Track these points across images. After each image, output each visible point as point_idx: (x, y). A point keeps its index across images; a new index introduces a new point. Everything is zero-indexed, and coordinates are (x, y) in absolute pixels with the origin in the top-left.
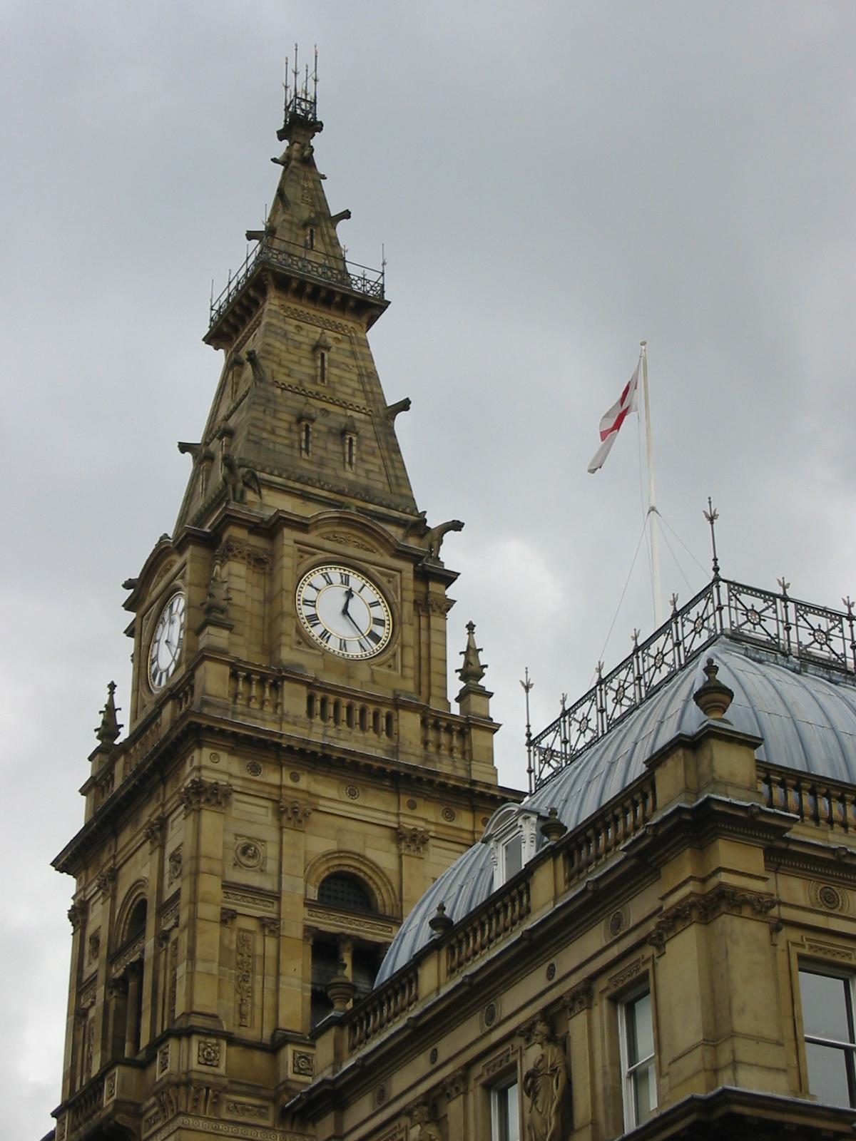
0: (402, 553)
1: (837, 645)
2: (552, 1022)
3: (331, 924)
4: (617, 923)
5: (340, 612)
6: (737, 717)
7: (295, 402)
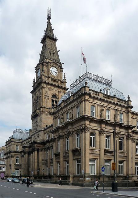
0: (59, 66)
1: (96, 78)
2: (72, 108)
3: (53, 99)
4: (77, 101)
5: (54, 71)
6: (88, 85)
7: (49, 50)
